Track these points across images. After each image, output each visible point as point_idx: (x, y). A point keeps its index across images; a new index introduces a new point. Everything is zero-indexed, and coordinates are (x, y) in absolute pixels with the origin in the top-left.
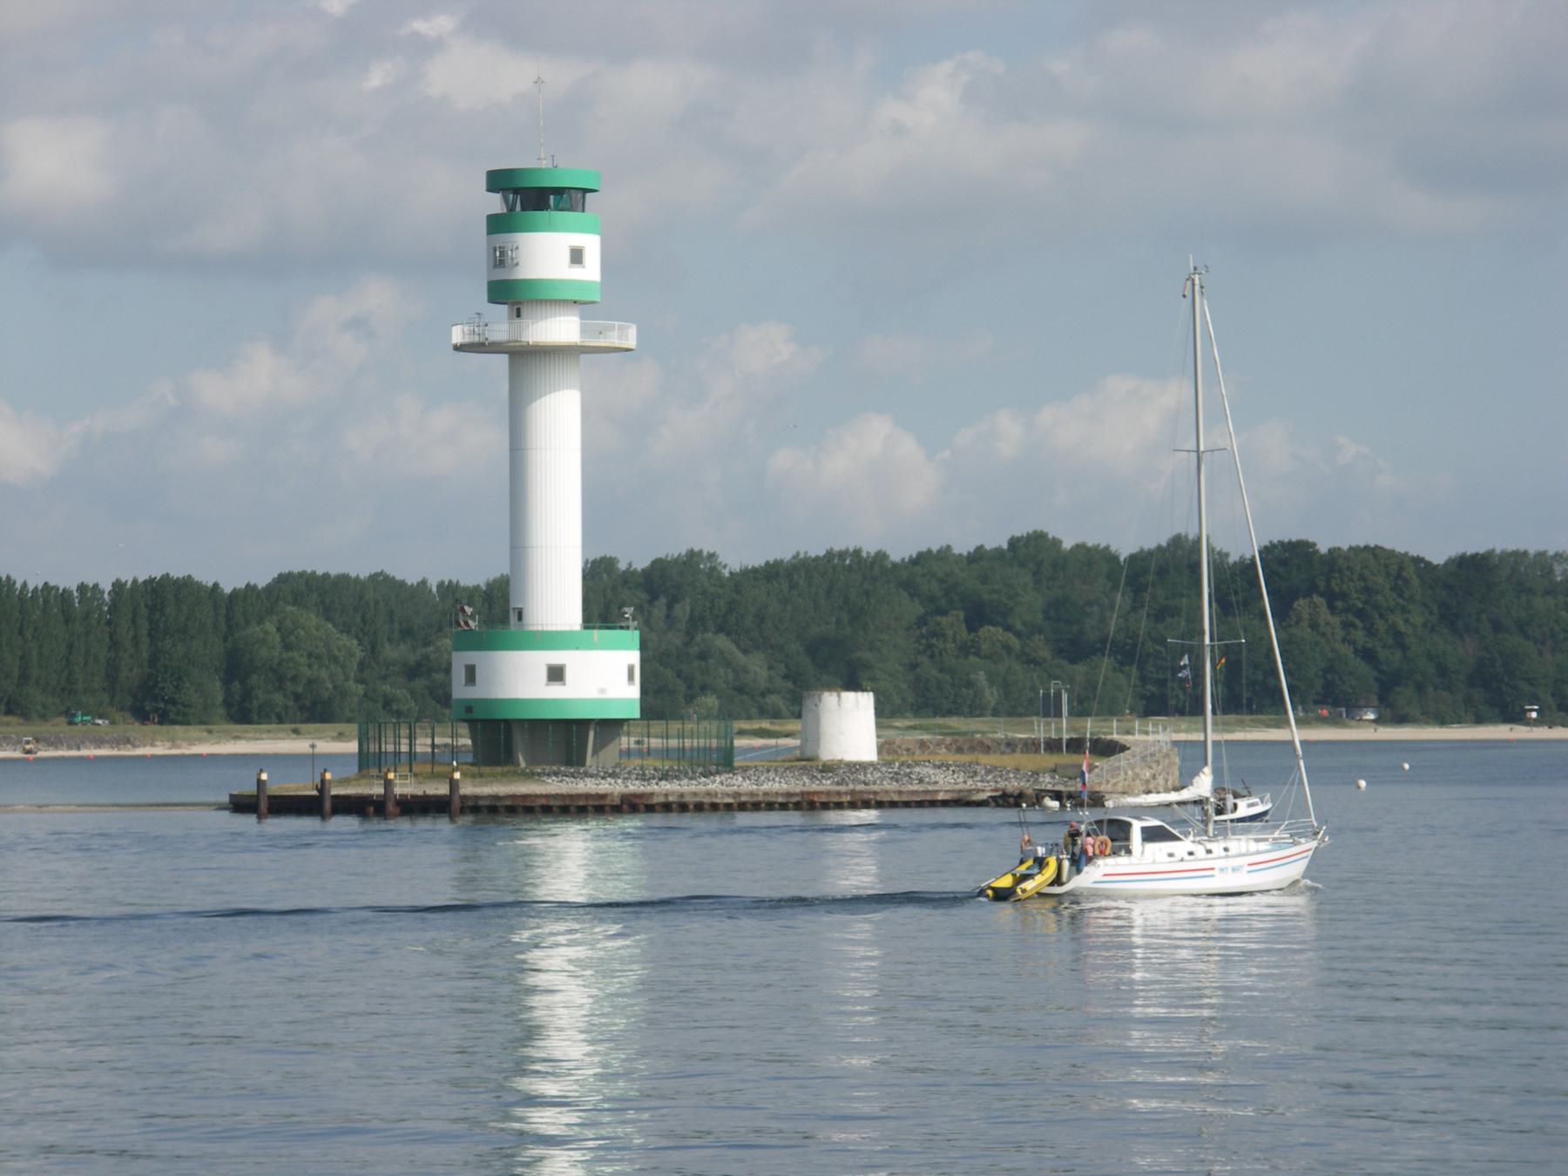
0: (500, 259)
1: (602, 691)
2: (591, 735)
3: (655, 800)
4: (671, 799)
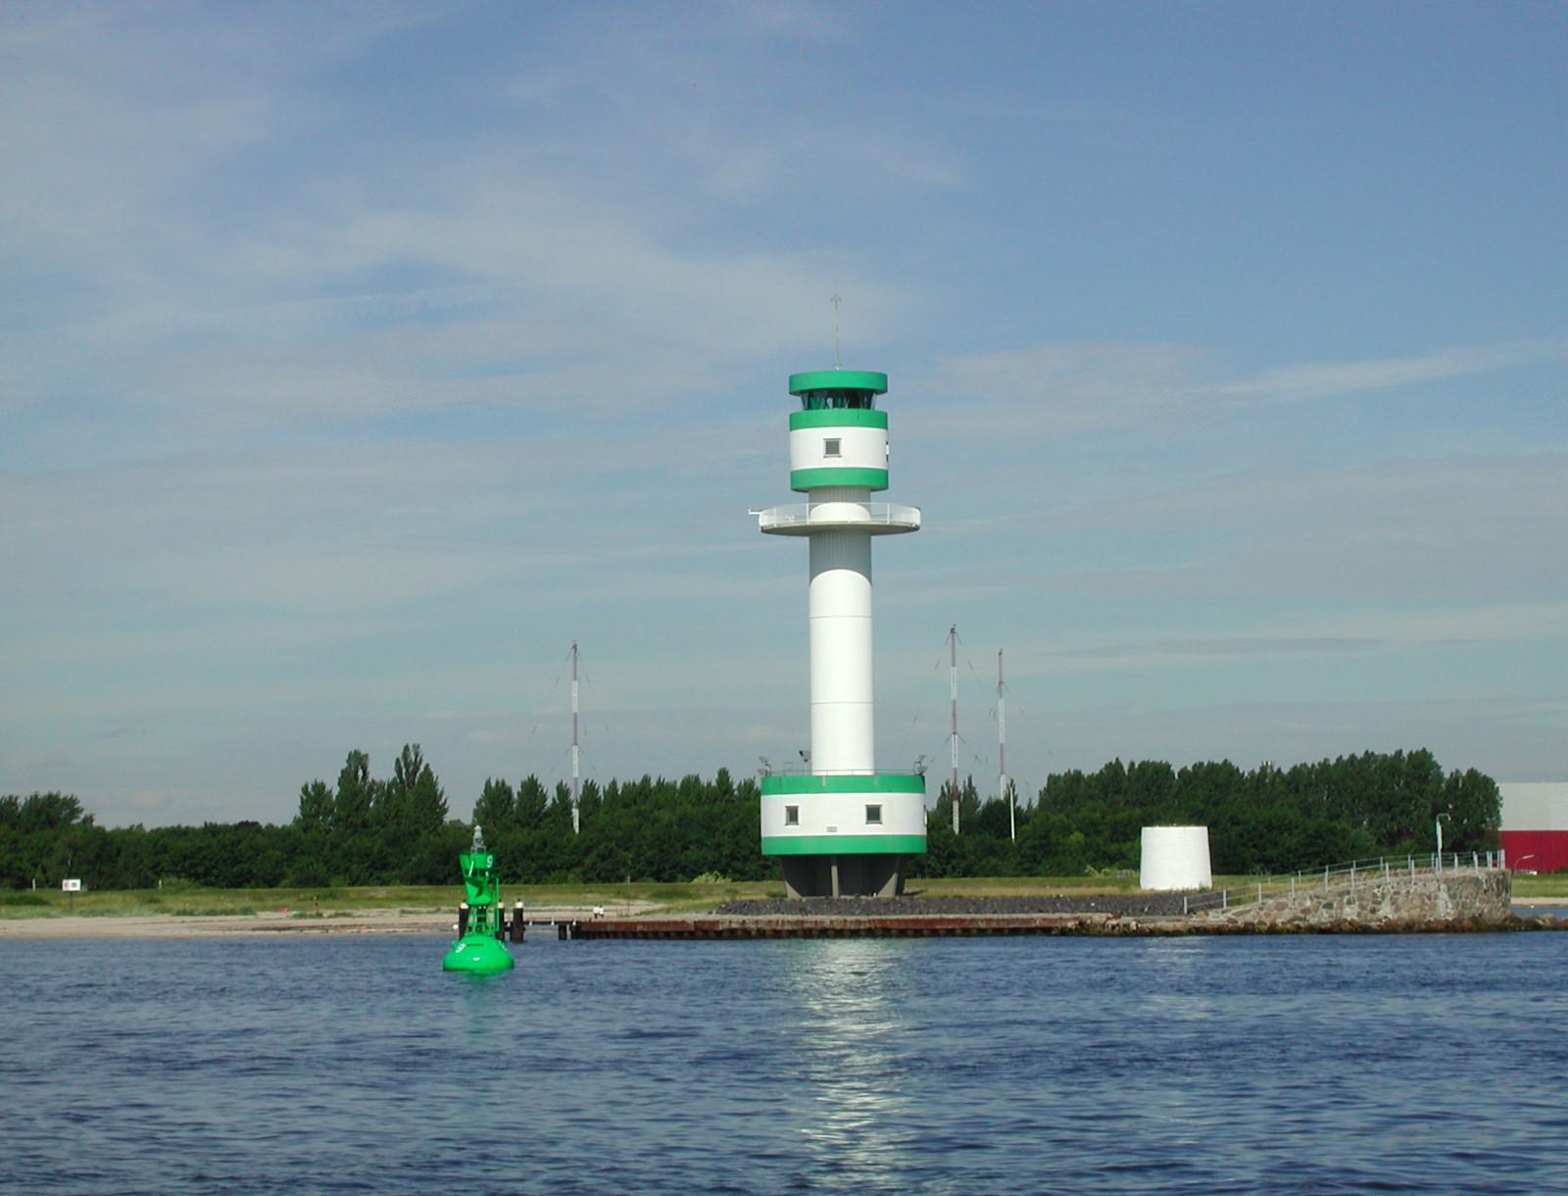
0: (786, 457)
1: (832, 829)
2: (834, 870)
3: (609, 929)
4: (734, 926)
